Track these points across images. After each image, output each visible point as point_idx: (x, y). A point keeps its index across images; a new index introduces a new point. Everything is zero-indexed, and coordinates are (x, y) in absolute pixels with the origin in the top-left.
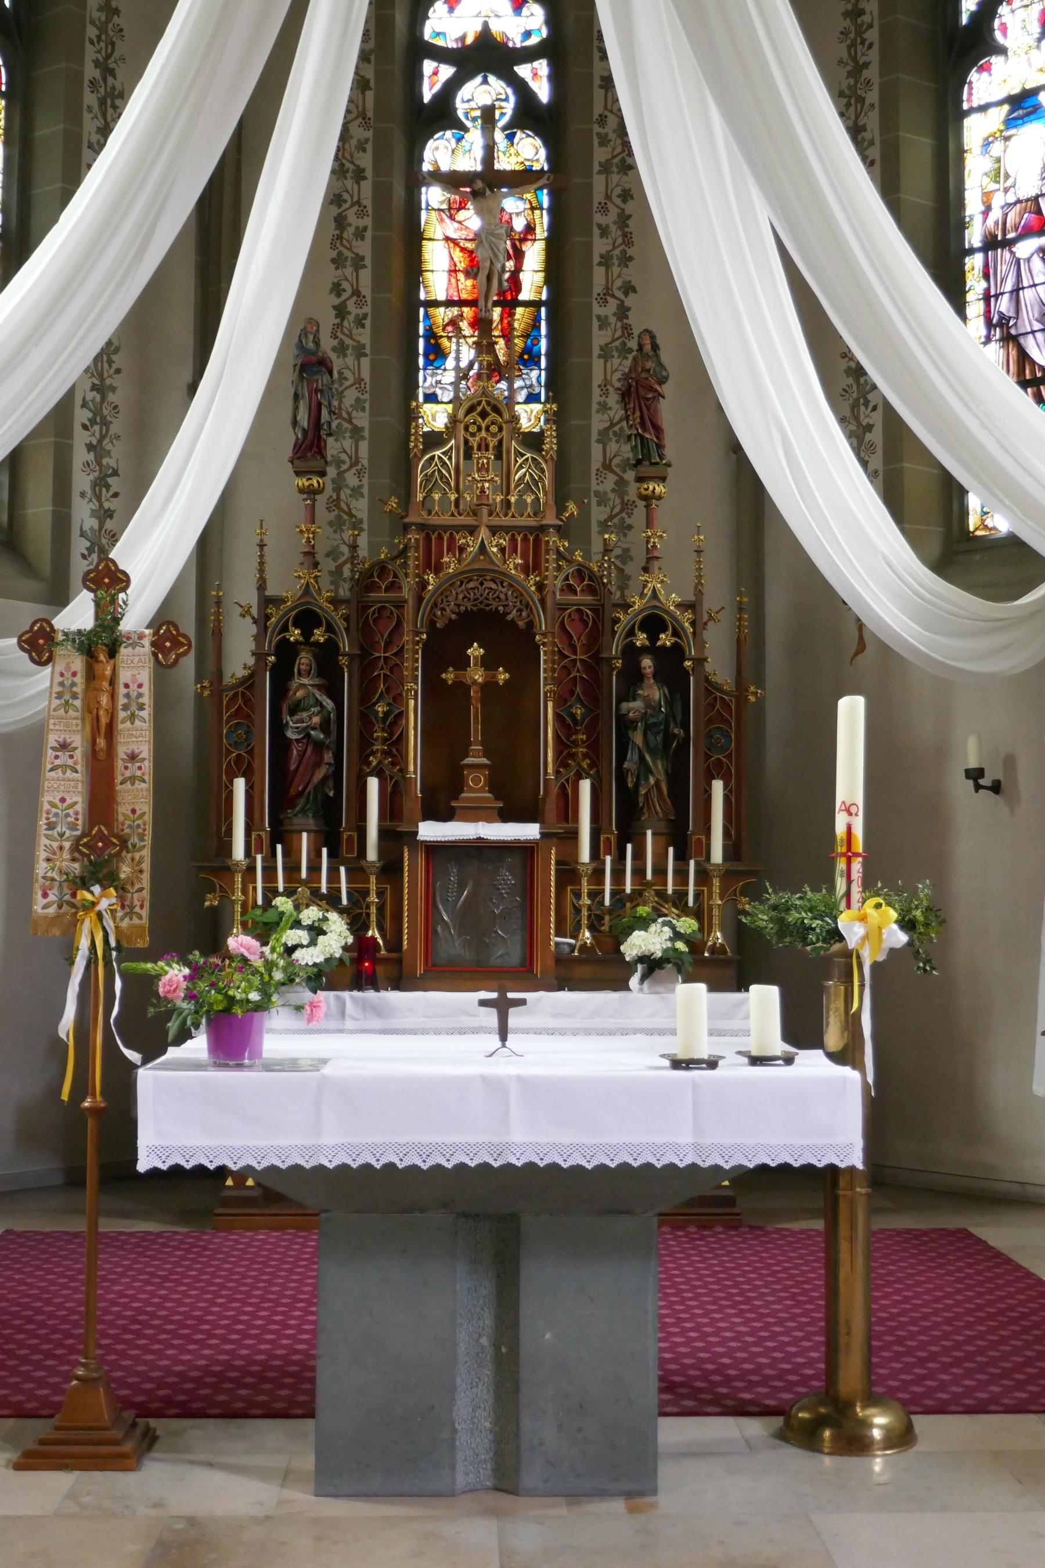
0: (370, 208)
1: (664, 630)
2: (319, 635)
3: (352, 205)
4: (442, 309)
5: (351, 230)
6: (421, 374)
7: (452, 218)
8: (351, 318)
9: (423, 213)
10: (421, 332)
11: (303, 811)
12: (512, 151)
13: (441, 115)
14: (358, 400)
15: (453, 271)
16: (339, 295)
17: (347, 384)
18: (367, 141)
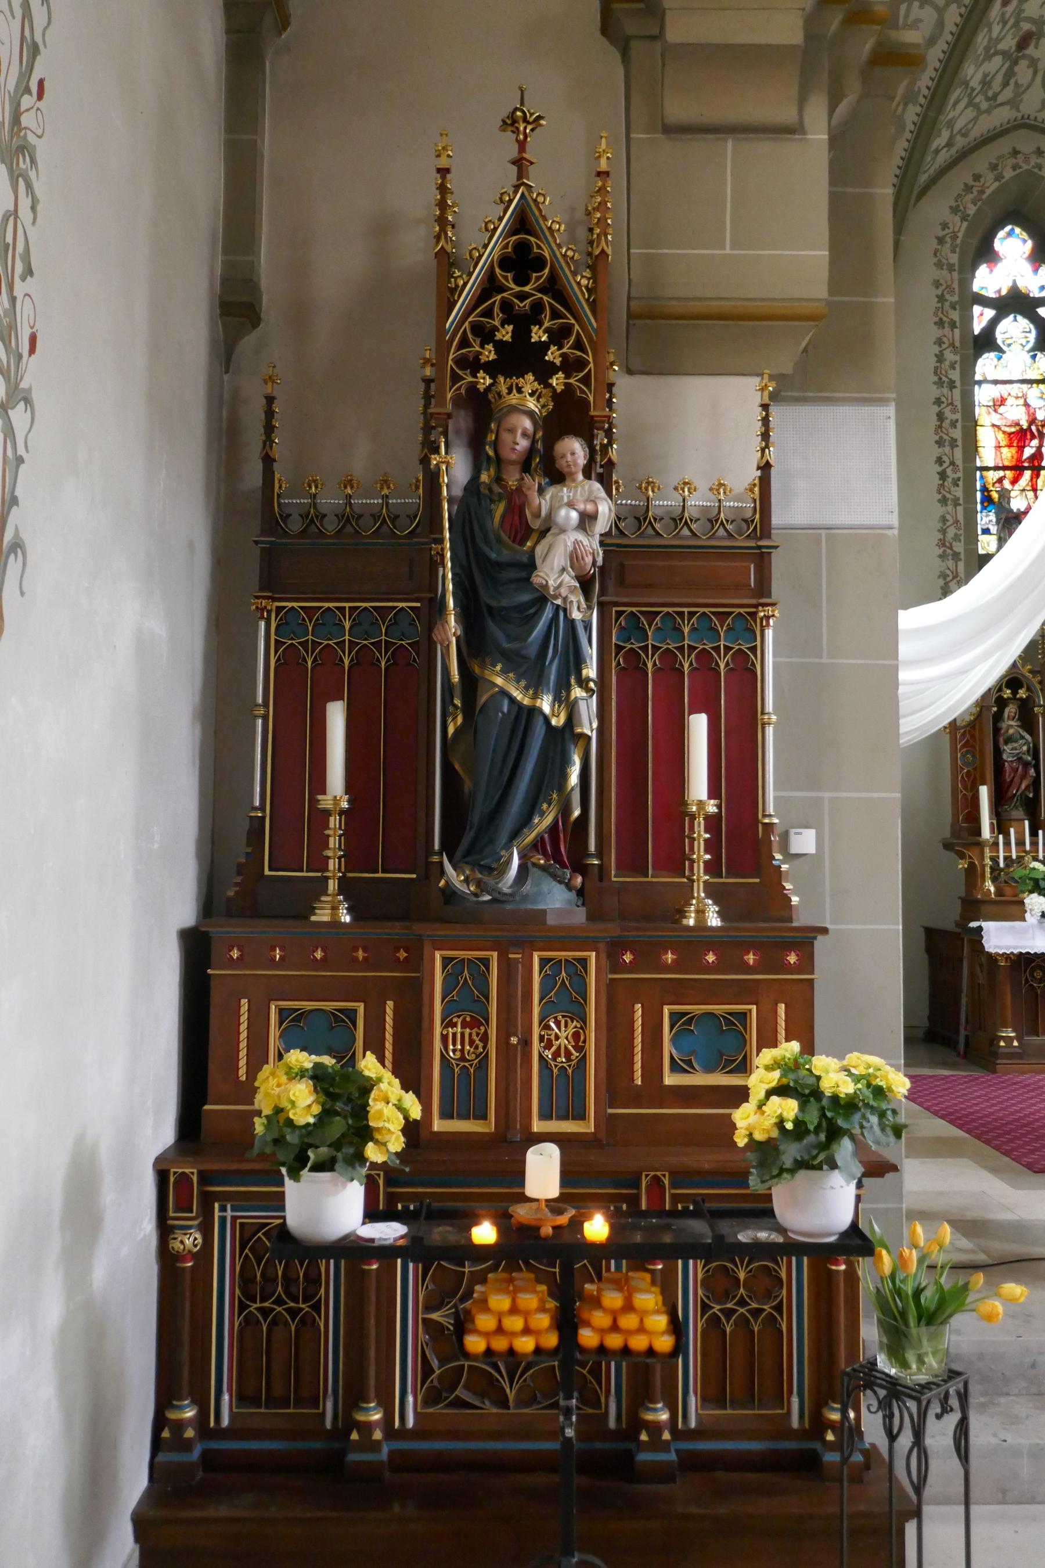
0: (959, 407)
1: (1021, 687)
2: (1022, 693)
3: (948, 405)
4: (991, 472)
5: (948, 422)
6: (979, 515)
7: (996, 411)
8: (950, 480)
9: (977, 408)
10: (978, 487)
11: (1015, 807)
12: (1035, 366)
13: (986, 342)
14: (956, 535)
15: (998, 447)
16: (941, 465)
17: (948, 524)
18: (956, 362)
